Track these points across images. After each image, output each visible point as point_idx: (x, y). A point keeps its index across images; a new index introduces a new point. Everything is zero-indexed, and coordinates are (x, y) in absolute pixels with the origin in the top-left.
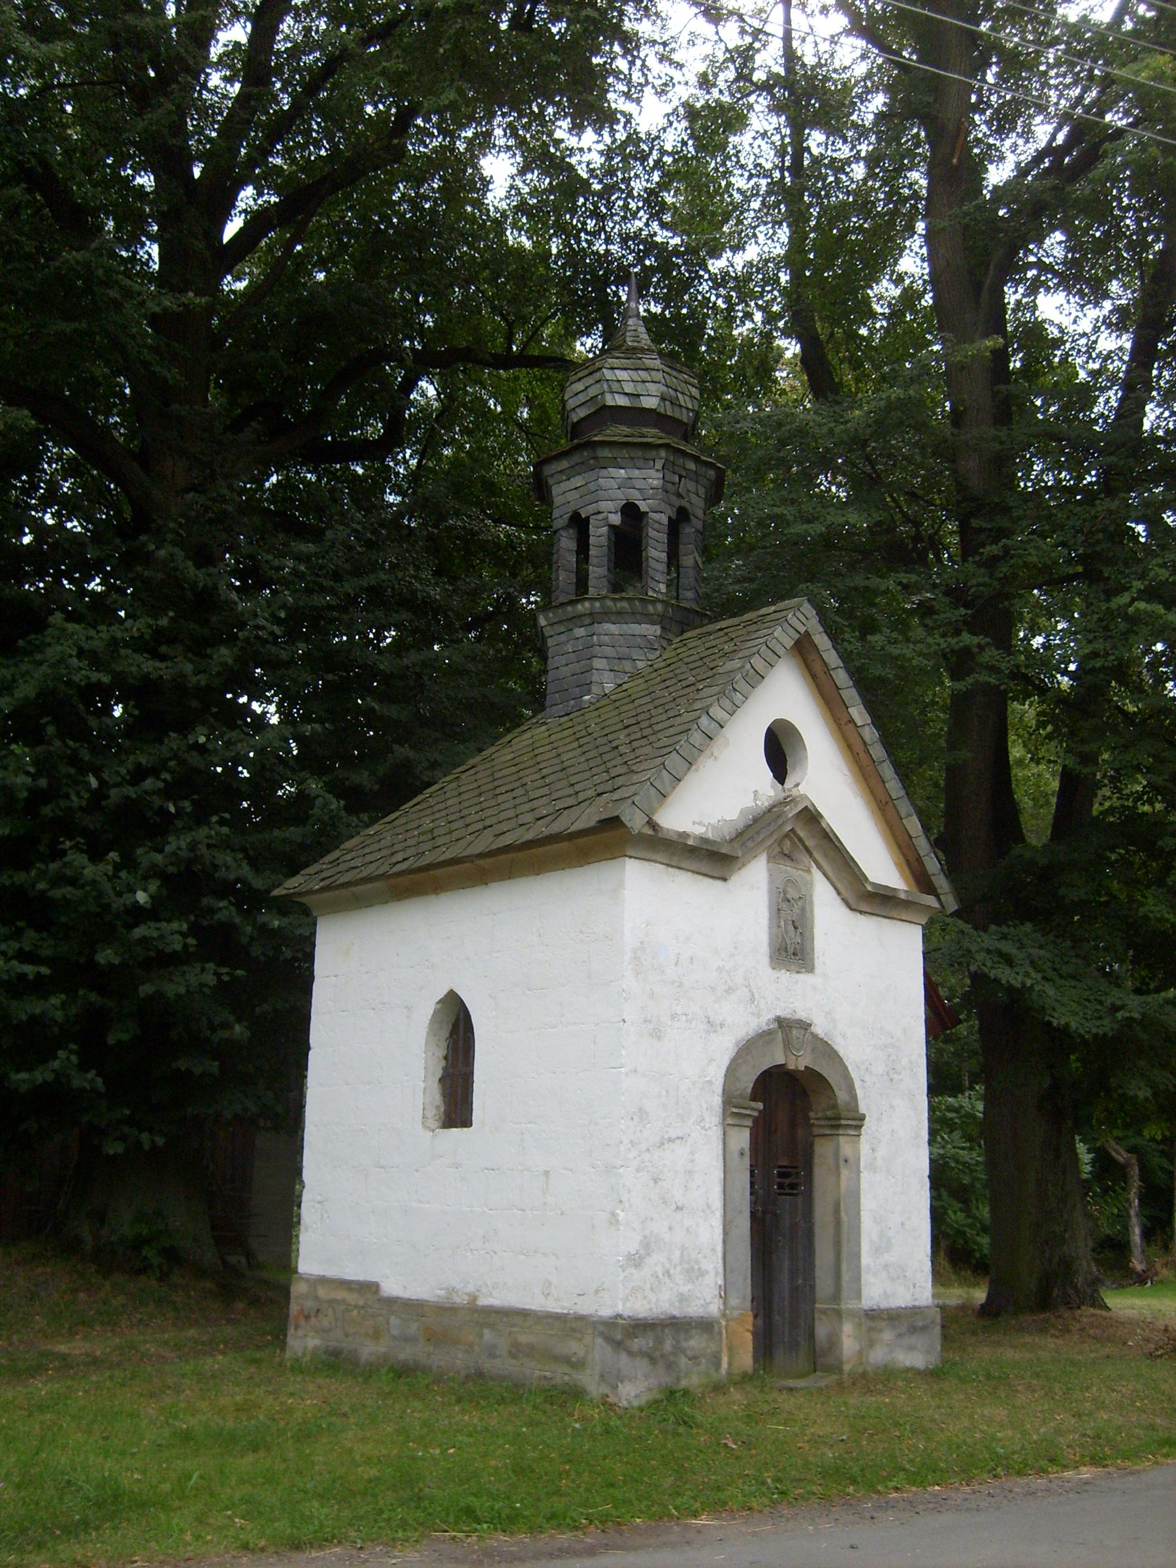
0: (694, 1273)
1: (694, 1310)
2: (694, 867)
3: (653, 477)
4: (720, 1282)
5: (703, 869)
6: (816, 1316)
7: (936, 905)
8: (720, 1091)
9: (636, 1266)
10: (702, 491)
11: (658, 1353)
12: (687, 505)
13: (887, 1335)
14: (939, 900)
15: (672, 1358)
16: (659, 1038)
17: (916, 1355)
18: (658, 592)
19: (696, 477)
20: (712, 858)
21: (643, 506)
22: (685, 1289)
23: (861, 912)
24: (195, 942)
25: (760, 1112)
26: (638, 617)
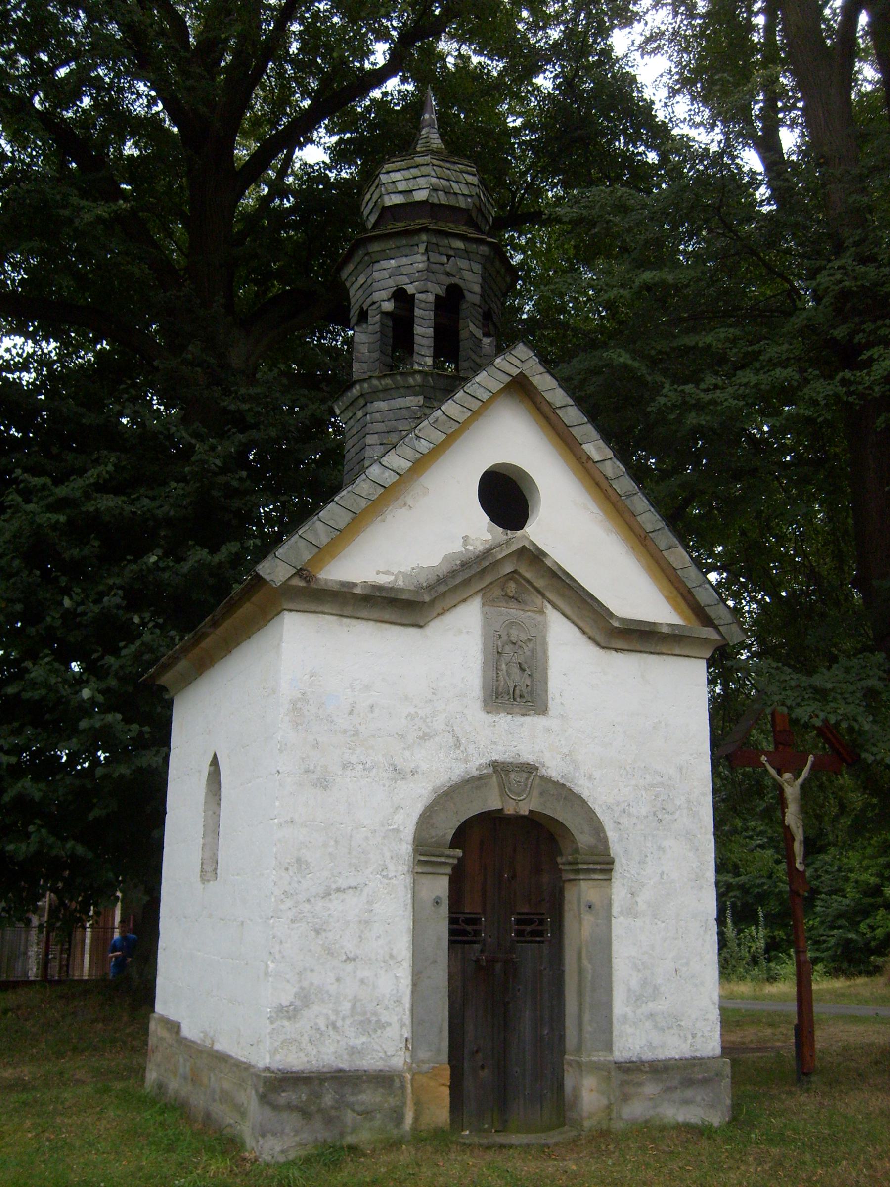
0: (370, 1024)
1: (370, 1062)
2: (376, 616)
3: (418, 261)
4: (407, 1033)
5: (387, 617)
6: (565, 1067)
7: (715, 636)
8: (410, 838)
9: (289, 1018)
10: (477, 268)
11: (313, 1108)
12: (461, 283)
13: (650, 1089)
14: (719, 632)
15: (333, 1113)
16: (325, 788)
17: (703, 1110)
18: (425, 365)
19: (467, 255)
20: (402, 605)
21: (411, 289)
22: (359, 1041)
23: (616, 650)
24: (149, 730)
25: (459, 859)
26: (402, 391)
